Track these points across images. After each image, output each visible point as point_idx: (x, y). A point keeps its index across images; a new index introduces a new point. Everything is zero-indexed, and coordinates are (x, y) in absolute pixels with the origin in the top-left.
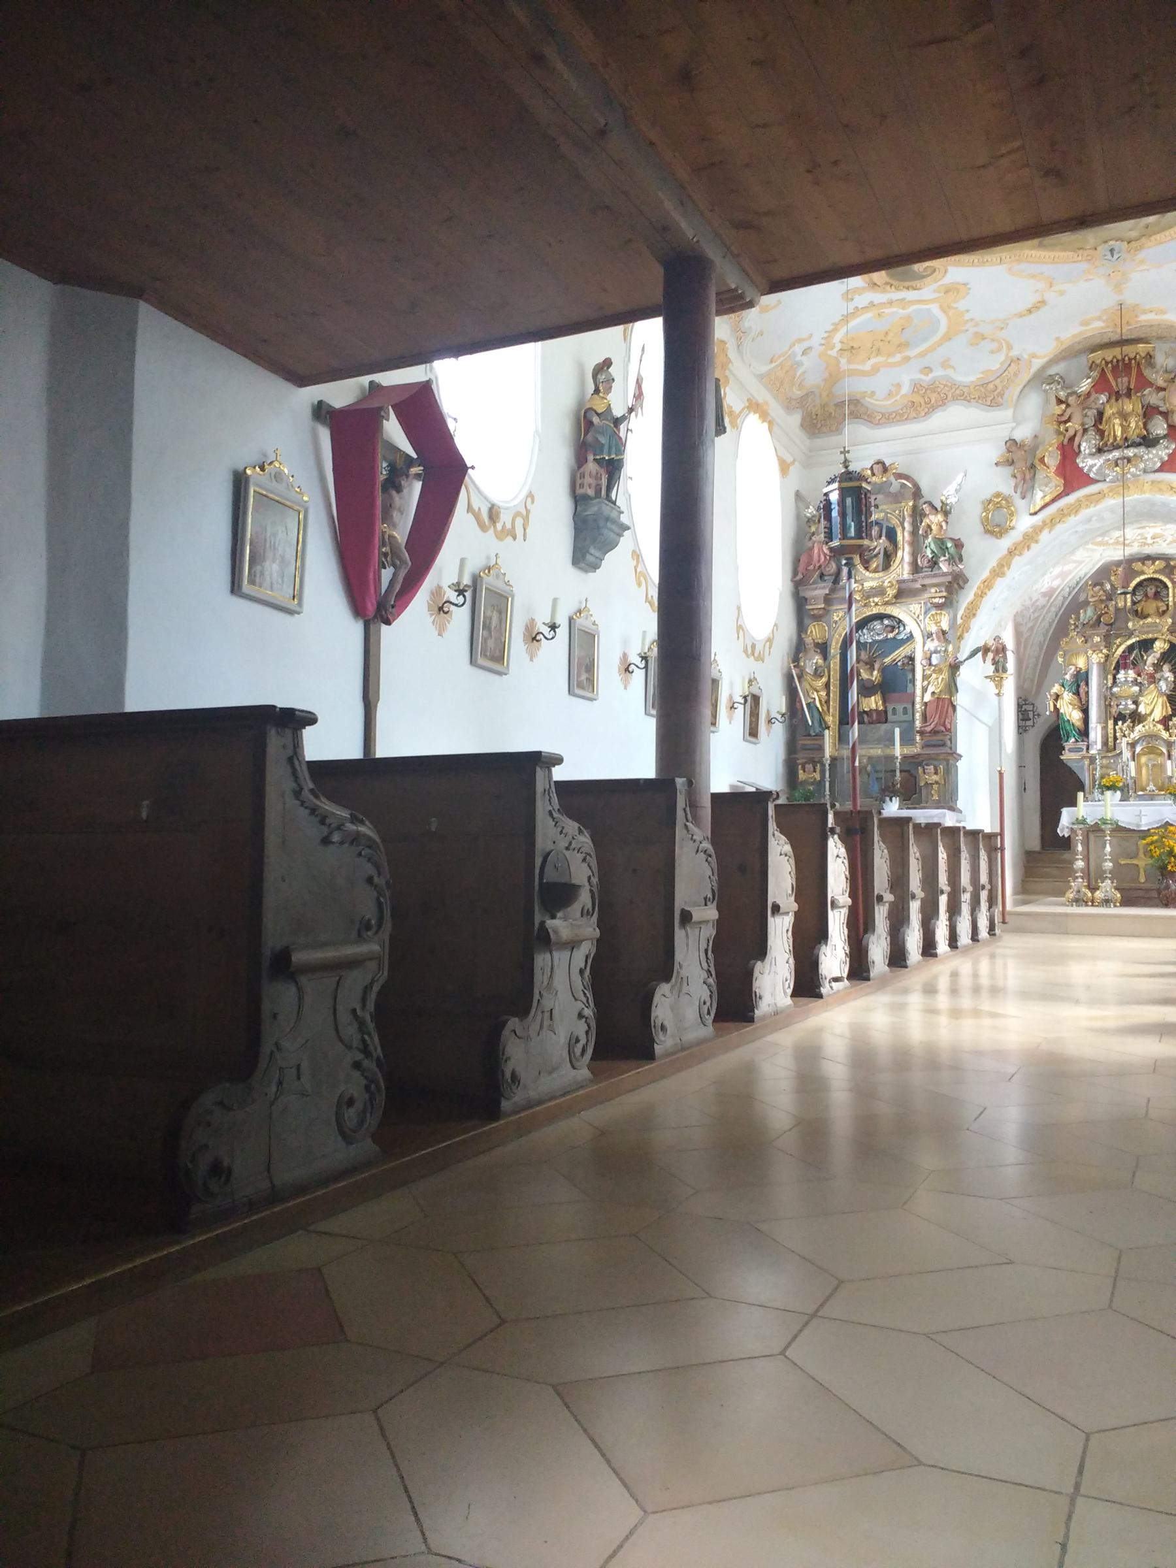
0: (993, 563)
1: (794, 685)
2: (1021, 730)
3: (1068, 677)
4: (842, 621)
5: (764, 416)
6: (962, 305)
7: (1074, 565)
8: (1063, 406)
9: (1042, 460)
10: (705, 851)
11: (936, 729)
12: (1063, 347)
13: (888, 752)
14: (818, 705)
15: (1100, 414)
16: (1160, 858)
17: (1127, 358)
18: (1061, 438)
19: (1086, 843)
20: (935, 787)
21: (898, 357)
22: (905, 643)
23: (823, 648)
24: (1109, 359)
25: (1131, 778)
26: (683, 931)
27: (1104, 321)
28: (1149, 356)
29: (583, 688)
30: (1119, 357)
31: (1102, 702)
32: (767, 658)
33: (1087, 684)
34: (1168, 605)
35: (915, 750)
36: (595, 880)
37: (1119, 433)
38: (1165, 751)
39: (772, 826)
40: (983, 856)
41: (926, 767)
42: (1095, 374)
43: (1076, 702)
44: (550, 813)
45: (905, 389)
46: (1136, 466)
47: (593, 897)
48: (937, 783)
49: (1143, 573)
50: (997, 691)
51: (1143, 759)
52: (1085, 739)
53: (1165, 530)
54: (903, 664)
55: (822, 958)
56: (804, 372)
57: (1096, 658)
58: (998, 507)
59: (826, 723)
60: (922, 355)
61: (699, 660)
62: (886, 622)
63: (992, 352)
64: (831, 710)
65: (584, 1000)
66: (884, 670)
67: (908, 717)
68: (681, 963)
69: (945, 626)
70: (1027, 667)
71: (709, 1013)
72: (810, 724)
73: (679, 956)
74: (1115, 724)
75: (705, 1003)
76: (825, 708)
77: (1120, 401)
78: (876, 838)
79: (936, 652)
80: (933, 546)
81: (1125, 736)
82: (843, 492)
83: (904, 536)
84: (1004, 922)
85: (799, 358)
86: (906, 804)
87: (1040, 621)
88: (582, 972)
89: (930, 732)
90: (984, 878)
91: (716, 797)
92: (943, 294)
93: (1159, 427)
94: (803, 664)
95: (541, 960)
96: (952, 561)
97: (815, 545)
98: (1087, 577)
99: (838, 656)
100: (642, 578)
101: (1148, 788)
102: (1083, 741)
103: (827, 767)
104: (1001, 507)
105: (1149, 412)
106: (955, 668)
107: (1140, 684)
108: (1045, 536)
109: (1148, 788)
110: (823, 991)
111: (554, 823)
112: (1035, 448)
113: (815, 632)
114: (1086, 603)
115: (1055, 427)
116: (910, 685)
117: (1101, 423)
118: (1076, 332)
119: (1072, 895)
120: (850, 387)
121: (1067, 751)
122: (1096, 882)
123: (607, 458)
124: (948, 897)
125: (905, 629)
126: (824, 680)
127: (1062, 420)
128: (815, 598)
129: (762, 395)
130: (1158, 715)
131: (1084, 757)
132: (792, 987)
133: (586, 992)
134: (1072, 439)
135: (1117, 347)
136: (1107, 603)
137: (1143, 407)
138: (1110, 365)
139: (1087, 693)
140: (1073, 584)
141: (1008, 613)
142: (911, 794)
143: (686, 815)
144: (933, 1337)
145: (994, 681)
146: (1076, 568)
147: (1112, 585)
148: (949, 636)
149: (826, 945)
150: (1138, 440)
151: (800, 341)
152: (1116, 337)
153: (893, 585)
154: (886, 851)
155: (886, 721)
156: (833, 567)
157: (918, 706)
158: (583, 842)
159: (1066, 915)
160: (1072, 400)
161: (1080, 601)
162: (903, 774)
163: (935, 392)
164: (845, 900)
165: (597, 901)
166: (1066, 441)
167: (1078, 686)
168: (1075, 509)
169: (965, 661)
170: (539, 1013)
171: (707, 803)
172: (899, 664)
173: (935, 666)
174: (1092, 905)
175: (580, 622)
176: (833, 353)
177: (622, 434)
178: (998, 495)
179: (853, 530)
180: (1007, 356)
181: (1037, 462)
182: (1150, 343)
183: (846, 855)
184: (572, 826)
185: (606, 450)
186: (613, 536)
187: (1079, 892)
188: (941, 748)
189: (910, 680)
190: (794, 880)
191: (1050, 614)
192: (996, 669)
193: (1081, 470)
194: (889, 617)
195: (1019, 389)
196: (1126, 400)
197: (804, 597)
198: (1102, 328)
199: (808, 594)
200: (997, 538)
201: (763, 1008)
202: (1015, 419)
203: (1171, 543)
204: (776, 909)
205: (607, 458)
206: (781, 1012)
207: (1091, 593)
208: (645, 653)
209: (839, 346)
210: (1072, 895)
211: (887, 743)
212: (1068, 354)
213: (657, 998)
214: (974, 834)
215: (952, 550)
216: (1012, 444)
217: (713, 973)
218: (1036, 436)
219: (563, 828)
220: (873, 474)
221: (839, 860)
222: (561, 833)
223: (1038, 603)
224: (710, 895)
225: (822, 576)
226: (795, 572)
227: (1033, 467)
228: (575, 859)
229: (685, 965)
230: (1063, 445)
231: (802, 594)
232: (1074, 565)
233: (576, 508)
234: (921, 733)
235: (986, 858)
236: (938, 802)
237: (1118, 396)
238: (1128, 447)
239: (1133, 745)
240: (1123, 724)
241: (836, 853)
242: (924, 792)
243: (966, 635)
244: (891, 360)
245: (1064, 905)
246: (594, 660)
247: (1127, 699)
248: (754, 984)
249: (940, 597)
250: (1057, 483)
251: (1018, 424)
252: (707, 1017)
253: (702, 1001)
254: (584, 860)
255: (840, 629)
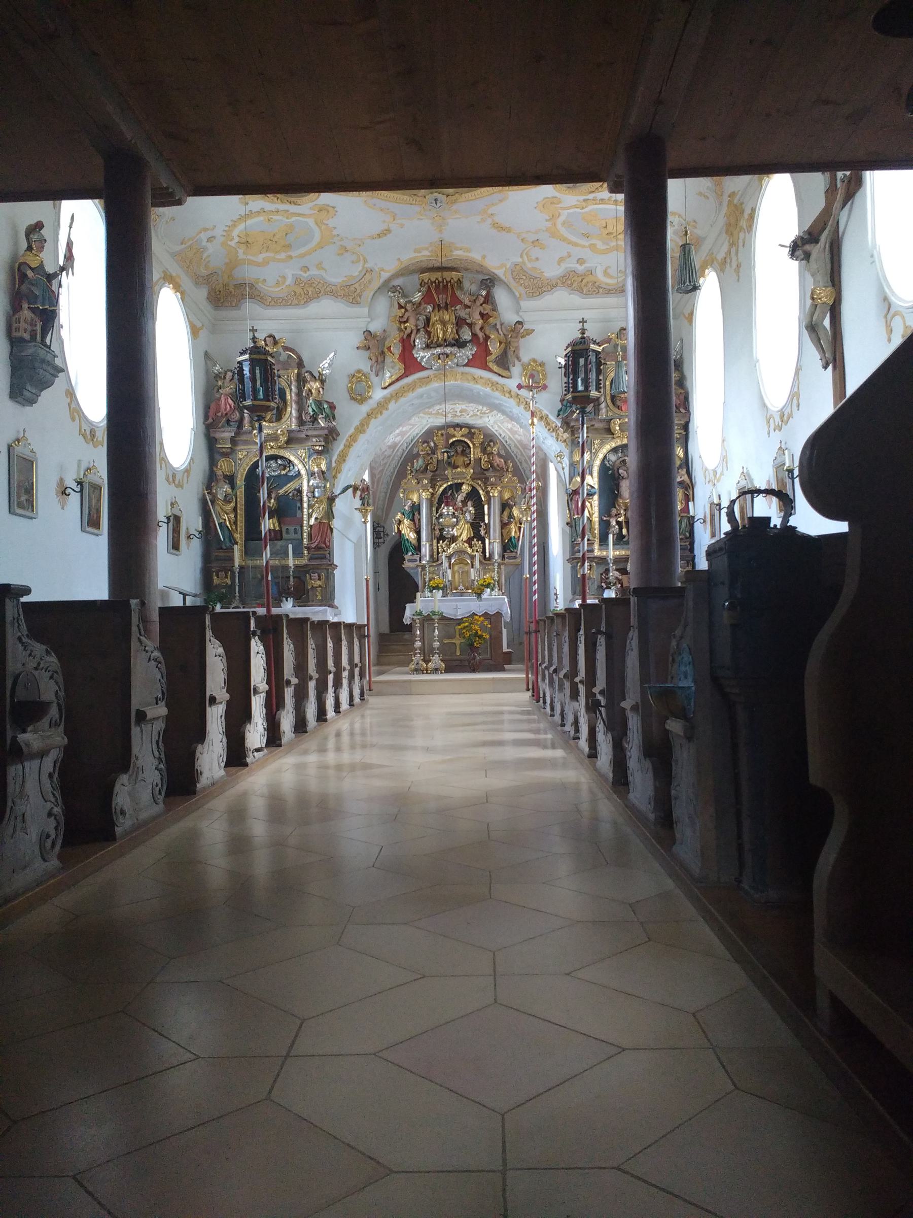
0: (356, 423)
1: (208, 508)
2: (375, 546)
3: (406, 508)
4: (246, 456)
5: (177, 288)
6: (331, 223)
7: (410, 427)
8: (403, 310)
9: (389, 348)
10: (156, 659)
11: (319, 546)
12: (403, 266)
13: (283, 562)
14: (228, 525)
15: (428, 320)
16: (469, 639)
17: (445, 281)
18: (402, 334)
19: (422, 631)
20: (319, 589)
21: (283, 256)
22: (295, 479)
23: (231, 480)
24: (433, 280)
25: (449, 581)
26: (138, 729)
27: (430, 252)
28: (459, 282)
29: (23, 508)
30: (440, 279)
31: (430, 527)
32: (185, 485)
33: (419, 514)
34: (470, 460)
35: (304, 561)
36: (62, 694)
37: (440, 336)
38: (469, 562)
39: (209, 633)
40: (356, 642)
41: (312, 575)
42: (424, 289)
43: (412, 526)
44: (20, 639)
45: (289, 281)
46: (451, 360)
47: (60, 710)
48: (320, 586)
49: (454, 436)
50: (363, 520)
51: (456, 568)
52: (419, 553)
53: (468, 406)
54: (293, 495)
55: (247, 735)
56: (209, 256)
57: (425, 495)
58: (359, 381)
59: (235, 539)
60: (302, 256)
61: (147, 498)
62: (279, 462)
63: (353, 262)
64: (238, 529)
65: (53, 800)
66: (278, 499)
67: (298, 536)
68: (137, 755)
69: (323, 467)
70: (379, 500)
71: (160, 793)
72: (222, 539)
73: (135, 750)
74: (438, 542)
75: (157, 785)
76: (234, 528)
77: (441, 312)
78: (285, 636)
79: (318, 487)
80: (313, 406)
81: (444, 551)
82: (253, 363)
83: (291, 396)
84: (370, 690)
85: (204, 243)
86: (298, 603)
87: (387, 466)
88: (51, 776)
89: (314, 548)
90: (357, 660)
91: (166, 612)
92: (316, 212)
93: (466, 335)
94: (215, 491)
95: (13, 771)
96: (327, 418)
97: (222, 396)
98: (418, 436)
99: (243, 486)
100: (75, 414)
101: (459, 588)
102: (417, 554)
103: (237, 574)
104: (361, 381)
105: (460, 323)
106: (331, 500)
107: (456, 517)
108: (392, 406)
109: (459, 588)
110: (248, 760)
111: (23, 647)
112: (384, 339)
113: (224, 466)
114: (417, 456)
115: (398, 325)
116: (299, 512)
117: (428, 326)
118: (411, 256)
119: (413, 666)
120: (249, 273)
121: (407, 562)
122: (429, 656)
123: (41, 308)
124: (334, 675)
125: (294, 468)
126: (232, 505)
127: (403, 321)
128: (223, 439)
129: (175, 270)
130: (464, 536)
131: (418, 566)
132: (225, 761)
133: (55, 792)
134: (409, 335)
135: (439, 271)
136: (432, 456)
137: (456, 318)
138: (434, 285)
139: (419, 520)
140: (409, 440)
141: (367, 459)
142: (302, 596)
143: (139, 630)
144: (380, 1054)
145: (361, 512)
146: (410, 429)
147: (435, 444)
148: (327, 476)
149: (250, 723)
150: (453, 342)
151: (206, 230)
152: (438, 264)
153: (284, 433)
154: (292, 645)
155: (281, 539)
156: (237, 415)
157: (305, 528)
158: (50, 662)
159: (410, 681)
160: (409, 306)
161: (414, 453)
162: (296, 579)
163: (311, 286)
164: (263, 687)
165: (64, 711)
166: (405, 336)
167: (414, 515)
168: (412, 387)
169: (339, 495)
170: (12, 819)
171: (155, 617)
172: (291, 495)
173: (317, 498)
174: (427, 673)
175: (19, 449)
176: (233, 244)
177: (54, 287)
178: (359, 371)
179: (261, 393)
180: (363, 267)
181: (386, 350)
182: (460, 272)
183: (264, 652)
184: (39, 648)
185: (40, 299)
186: (49, 376)
187: (418, 664)
188: (323, 560)
189: (299, 508)
190: (226, 675)
191: (394, 462)
192: (362, 502)
193: (416, 359)
194: (282, 458)
195: (372, 294)
196: (445, 312)
197: (214, 438)
198: (429, 256)
199: (217, 435)
200: (360, 404)
201: (204, 781)
202: (370, 315)
203: (472, 416)
204: (213, 700)
205: (41, 308)
206: (217, 782)
207: (421, 448)
208: (81, 479)
209: (237, 239)
210: (413, 666)
211: (282, 555)
212: (405, 272)
213: (117, 787)
214: (349, 626)
215: (328, 411)
216: (368, 334)
217: (164, 760)
218: (384, 331)
219: (32, 651)
220: (266, 345)
221: (259, 656)
222: (30, 655)
223: (386, 453)
224: (160, 696)
225: (228, 422)
226: (206, 417)
227: (383, 353)
228: (43, 677)
229: (140, 756)
230: (403, 340)
231: (212, 435)
232: (410, 427)
233: (12, 349)
234: (308, 548)
235: (358, 643)
236: (321, 601)
237: (439, 308)
238: (446, 346)
239: (449, 558)
240: (443, 543)
241: (256, 647)
242: (310, 593)
243: (339, 475)
244: (278, 257)
245: (407, 673)
246: (33, 482)
247: (448, 527)
248: (196, 762)
249: (320, 446)
250: (399, 368)
251: (372, 320)
252: (159, 797)
253: (155, 784)
254: (51, 677)
255: (244, 465)
